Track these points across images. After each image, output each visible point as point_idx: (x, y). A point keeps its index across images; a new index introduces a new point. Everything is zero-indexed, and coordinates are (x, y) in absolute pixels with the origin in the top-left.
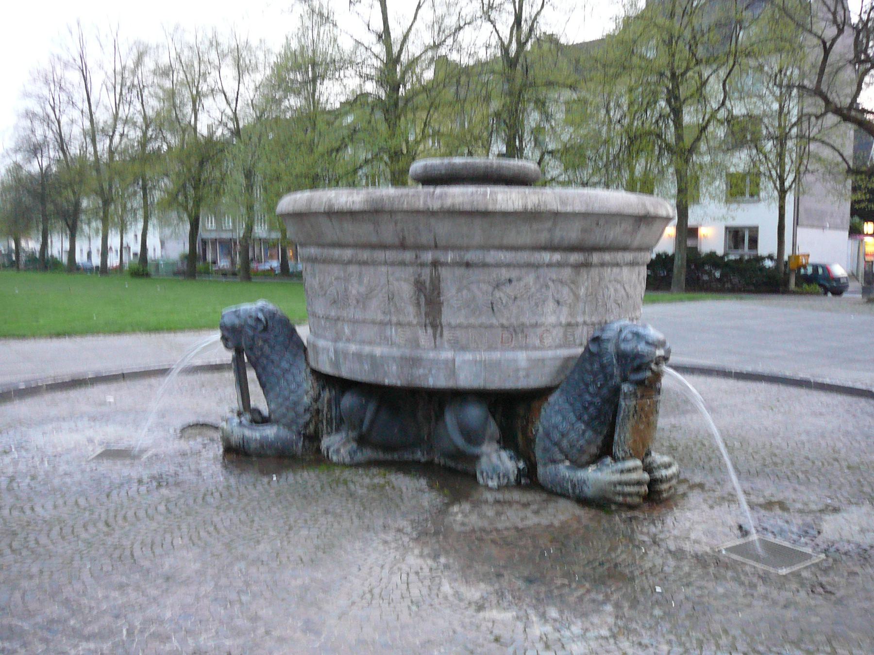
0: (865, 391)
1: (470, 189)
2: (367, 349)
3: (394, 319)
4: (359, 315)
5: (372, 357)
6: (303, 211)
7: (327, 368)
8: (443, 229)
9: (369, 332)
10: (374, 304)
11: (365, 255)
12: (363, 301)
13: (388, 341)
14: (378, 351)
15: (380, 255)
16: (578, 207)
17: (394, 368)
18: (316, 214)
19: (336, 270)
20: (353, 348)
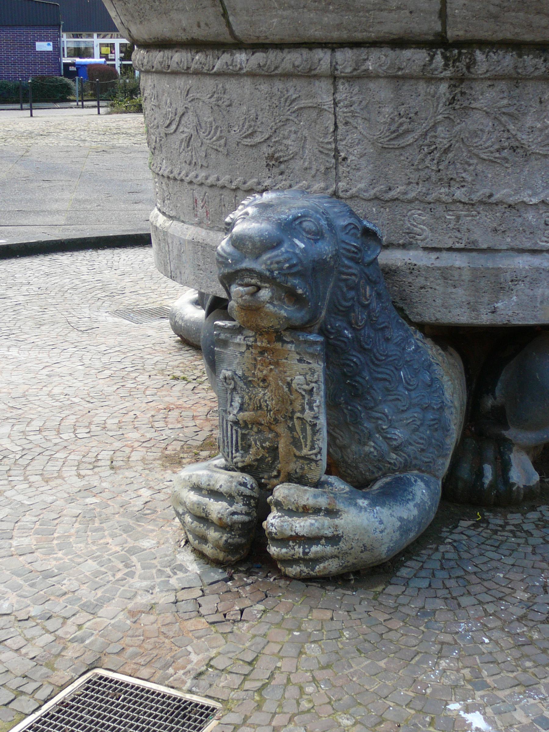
7: (459, 313)
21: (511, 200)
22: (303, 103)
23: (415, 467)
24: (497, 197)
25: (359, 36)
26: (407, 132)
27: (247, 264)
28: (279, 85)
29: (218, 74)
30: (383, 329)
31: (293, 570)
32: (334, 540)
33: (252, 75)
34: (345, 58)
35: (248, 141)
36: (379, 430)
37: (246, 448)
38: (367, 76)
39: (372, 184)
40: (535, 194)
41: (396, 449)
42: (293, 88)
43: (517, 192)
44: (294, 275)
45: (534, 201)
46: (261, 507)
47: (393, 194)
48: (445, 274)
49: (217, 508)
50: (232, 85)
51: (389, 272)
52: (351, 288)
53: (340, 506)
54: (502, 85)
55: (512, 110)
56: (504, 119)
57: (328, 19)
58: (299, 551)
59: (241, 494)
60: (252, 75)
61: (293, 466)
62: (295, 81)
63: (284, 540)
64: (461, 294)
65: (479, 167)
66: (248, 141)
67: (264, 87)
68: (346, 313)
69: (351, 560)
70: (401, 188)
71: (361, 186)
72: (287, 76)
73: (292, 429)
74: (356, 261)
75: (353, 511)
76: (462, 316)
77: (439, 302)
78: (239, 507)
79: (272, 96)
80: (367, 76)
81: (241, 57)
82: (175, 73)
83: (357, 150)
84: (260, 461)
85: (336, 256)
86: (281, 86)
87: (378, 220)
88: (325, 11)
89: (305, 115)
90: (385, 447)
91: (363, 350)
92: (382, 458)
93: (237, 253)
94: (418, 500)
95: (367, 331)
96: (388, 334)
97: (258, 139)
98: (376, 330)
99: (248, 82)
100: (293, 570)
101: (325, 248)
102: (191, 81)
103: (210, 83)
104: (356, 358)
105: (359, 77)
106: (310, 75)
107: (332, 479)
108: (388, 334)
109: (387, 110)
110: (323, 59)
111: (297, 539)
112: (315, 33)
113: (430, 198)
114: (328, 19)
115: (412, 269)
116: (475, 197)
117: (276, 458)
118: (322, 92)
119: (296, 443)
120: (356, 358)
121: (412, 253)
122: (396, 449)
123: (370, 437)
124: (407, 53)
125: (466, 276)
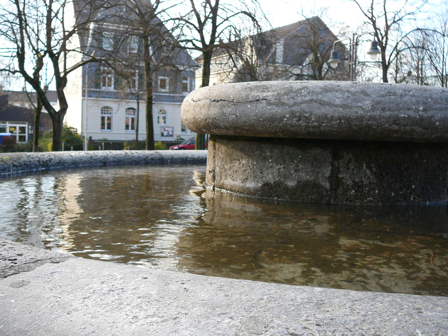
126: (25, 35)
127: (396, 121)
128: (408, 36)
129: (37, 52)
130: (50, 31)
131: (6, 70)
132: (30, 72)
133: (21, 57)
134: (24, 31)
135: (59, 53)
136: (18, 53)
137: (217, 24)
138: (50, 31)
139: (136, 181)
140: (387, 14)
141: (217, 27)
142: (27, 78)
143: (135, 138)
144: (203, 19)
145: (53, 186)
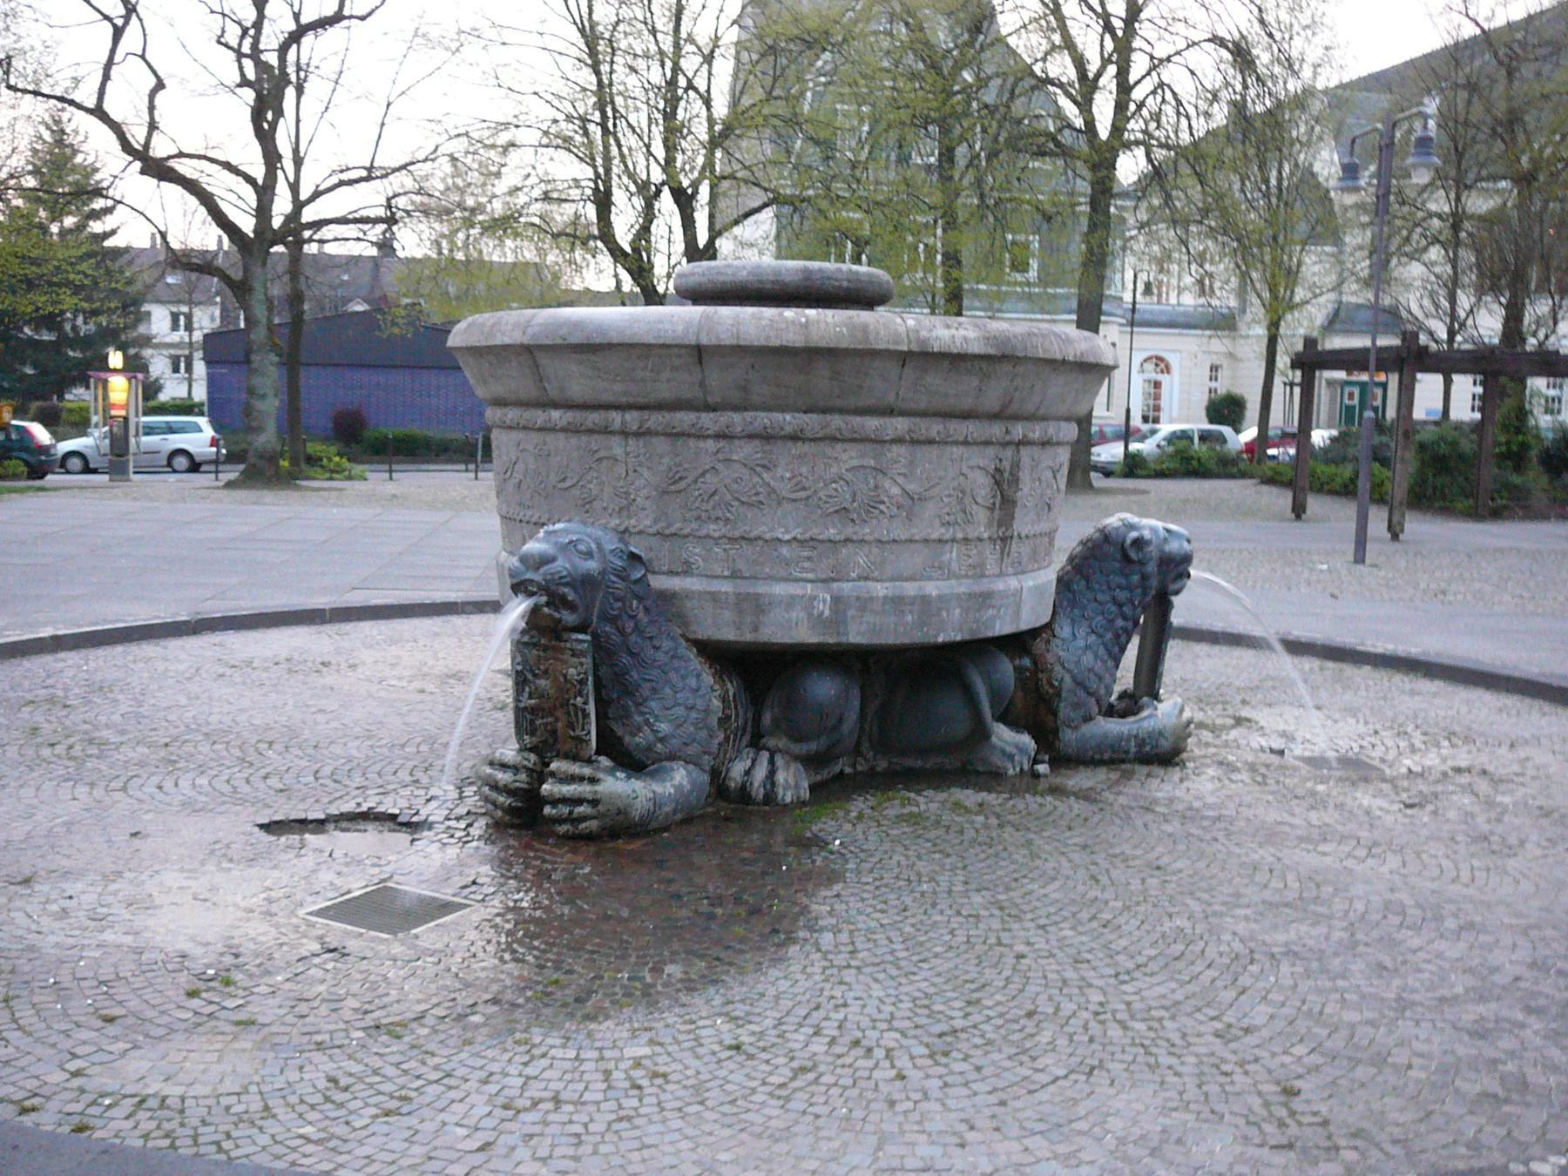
0: (31, 654)
1: (769, 312)
2: (910, 589)
3: (960, 536)
4: (900, 532)
5: (924, 600)
6: (844, 345)
7: (726, 631)
8: (880, 386)
9: (915, 559)
10: (929, 510)
11: (935, 428)
12: (911, 504)
13: (947, 573)
14: (932, 589)
15: (971, 429)
16: (517, 338)
17: (957, 611)
18: (874, 354)
19: (849, 456)
20: (880, 590)
21: (768, 536)
22: (602, 454)
23: (680, 758)
24: (754, 534)
25: (641, 400)
26: (681, 478)
27: (529, 576)
28: (584, 438)
29: (540, 429)
30: (651, 638)
31: (563, 829)
32: (594, 802)
33: (564, 430)
34: (632, 418)
35: (562, 485)
36: (647, 722)
37: (532, 734)
38: (649, 433)
39: (655, 521)
40: (787, 532)
41: (661, 740)
42: (595, 441)
43: (772, 530)
44: (566, 585)
45: (787, 537)
46: (539, 775)
47: (673, 530)
48: (714, 597)
49: (503, 777)
50: (550, 437)
51: (667, 597)
52: (617, 600)
53: (601, 775)
54: (757, 442)
55: (765, 462)
56: (759, 469)
57: (618, 387)
58: (565, 810)
59: (525, 767)
60: (564, 430)
61: (569, 746)
62: (596, 436)
63: (555, 802)
64: (728, 615)
65: (741, 510)
66: (562, 485)
67: (574, 441)
68: (613, 620)
69: (608, 822)
70: (678, 525)
71: (648, 522)
72: (590, 431)
73: (568, 714)
74: (623, 579)
75: (610, 779)
76: (728, 634)
77: (710, 621)
78: (523, 776)
79: (579, 448)
80: (649, 433)
81: (555, 414)
82: (510, 428)
83: (644, 492)
84: (545, 742)
85: (603, 573)
86: (941, 427)
87: (660, 553)
88: (614, 381)
89: (605, 463)
90: (651, 738)
91: (631, 653)
92: (649, 748)
93: (522, 568)
94: (676, 782)
95: (633, 638)
96: (656, 643)
97: (568, 483)
98: (644, 638)
99: (561, 436)
100: (563, 829)
101: (592, 565)
102: (521, 435)
103: (534, 436)
104: (625, 659)
105: (644, 434)
106: (606, 431)
107: (601, 758)
108: (656, 643)
109: (666, 460)
110: (616, 418)
111: (565, 800)
112: (606, 397)
113: (700, 533)
114: (618, 387)
115: (688, 595)
116: (737, 534)
117: (556, 740)
118: (617, 447)
119: (571, 726)
120: (625, 659)
121: (689, 580)
122: (661, 740)
123: (639, 730)
124: (679, 415)
125: (731, 600)
126: (614, 150)
127: (760, 282)
128: (91, 103)
129: (643, 187)
130: (673, 133)
131: (567, 235)
132: (624, 239)
133: (603, 202)
134: (612, 141)
135: (695, 185)
136: (596, 190)
137: (1132, 80)
138: (673, 133)
139: (1194, 463)
140: (104, 59)
141: (1131, 88)
142: (616, 252)
143: (184, 394)
144: (1092, 69)
145: (1545, 479)
